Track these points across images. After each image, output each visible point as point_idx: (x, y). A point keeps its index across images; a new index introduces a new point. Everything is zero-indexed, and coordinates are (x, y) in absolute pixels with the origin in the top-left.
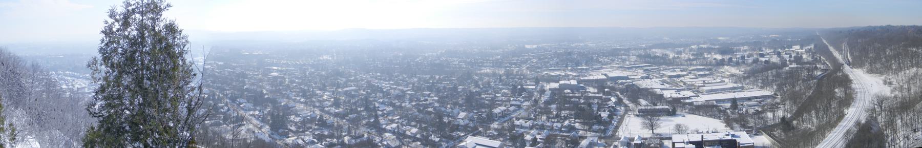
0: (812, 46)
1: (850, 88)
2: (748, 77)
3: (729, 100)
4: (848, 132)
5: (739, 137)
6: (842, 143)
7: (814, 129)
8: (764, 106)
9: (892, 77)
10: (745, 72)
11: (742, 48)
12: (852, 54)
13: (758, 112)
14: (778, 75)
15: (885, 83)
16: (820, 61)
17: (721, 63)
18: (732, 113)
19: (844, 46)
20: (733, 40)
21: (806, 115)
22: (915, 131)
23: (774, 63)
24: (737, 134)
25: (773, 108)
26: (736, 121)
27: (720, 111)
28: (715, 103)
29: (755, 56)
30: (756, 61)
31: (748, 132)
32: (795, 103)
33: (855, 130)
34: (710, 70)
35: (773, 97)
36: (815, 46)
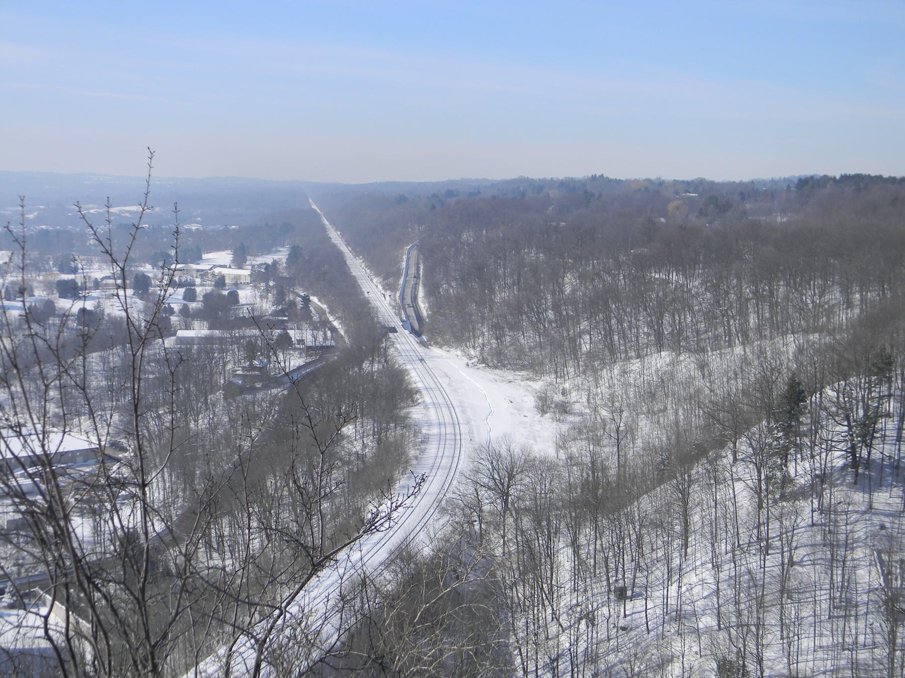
0: (281, 256)
1: (403, 422)
9: (576, 389)
12: (432, 291)
14: (133, 369)
15: (544, 405)
16: (304, 316)
19: (408, 258)
22: (622, 595)
25: (102, 492)
29: (40, 293)
36: (294, 255)
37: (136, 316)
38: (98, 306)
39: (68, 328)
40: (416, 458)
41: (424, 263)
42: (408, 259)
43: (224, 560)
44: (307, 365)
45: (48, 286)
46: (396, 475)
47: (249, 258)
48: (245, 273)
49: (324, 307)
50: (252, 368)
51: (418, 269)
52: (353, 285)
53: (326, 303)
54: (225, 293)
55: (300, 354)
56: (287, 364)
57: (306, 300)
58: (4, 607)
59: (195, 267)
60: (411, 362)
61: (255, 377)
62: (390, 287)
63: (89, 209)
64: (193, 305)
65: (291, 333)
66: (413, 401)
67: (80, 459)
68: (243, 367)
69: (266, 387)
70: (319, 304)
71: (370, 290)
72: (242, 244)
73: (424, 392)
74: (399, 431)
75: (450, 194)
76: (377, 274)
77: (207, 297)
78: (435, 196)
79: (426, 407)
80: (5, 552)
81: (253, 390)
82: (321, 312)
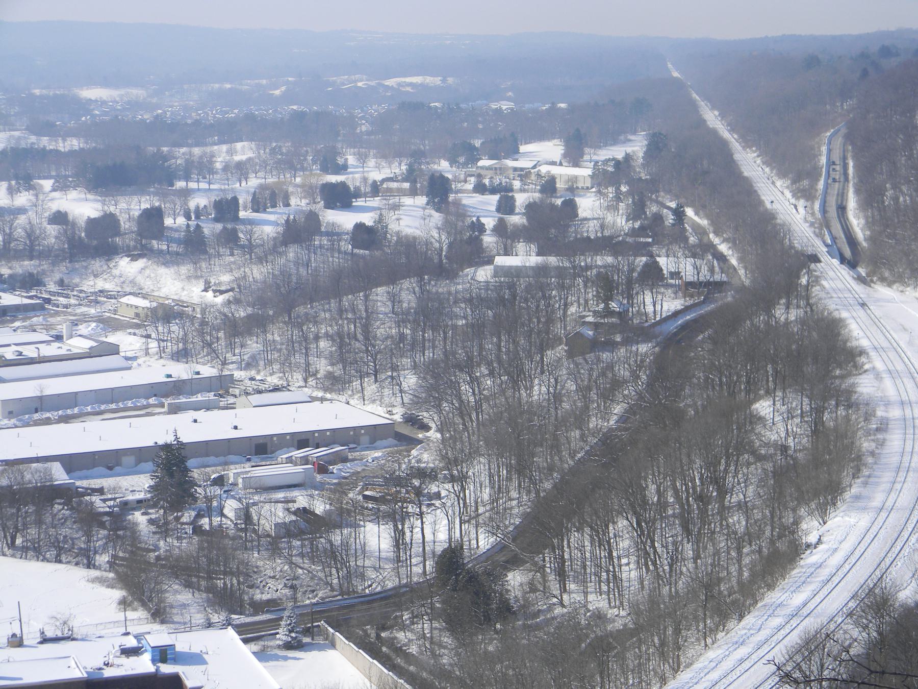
0: (636, 146)
1: (847, 399)
2: (256, 324)
3: (140, 455)
4: (813, 645)
5: (196, 659)
6: (911, 292)
7: (619, 617)
8: (341, 489)
10: (240, 291)
11: (221, 154)
12: (871, 199)
13: (308, 524)
14: (430, 314)
16: (676, 235)
17: (97, 243)
18: (163, 529)
19: (827, 147)
20: (172, 106)
21: (578, 543)
23: (409, 245)
24: (184, 643)
25: (398, 497)
26: (184, 571)
27: (90, 519)
28: (60, 475)
29: (299, 203)
30: (301, 231)
31: (249, 634)
32: (522, 469)
33: (857, 637)
34: (30, 282)
35: (400, 436)
36: (655, 147)
37: (436, 235)
38: (380, 220)
39: (339, 252)
40: (872, 454)
41: (856, 158)
42: (830, 151)
43: (586, 593)
44: (687, 309)
45: (309, 191)
46: (846, 481)
47: (587, 150)
48: (584, 172)
49: (704, 222)
50: (608, 313)
51: (845, 167)
52: (746, 193)
53: (707, 217)
54: (559, 202)
55: (675, 293)
56: (658, 307)
57: (679, 214)
58: (279, 647)
59: (510, 163)
60: (847, 307)
61: (613, 325)
62: (807, 194)
63: (356, 81)
64: (516, 219)
65: (662, 261)
66: (855, 366)
67: (365, 439)
68: (594, 312)
69: (627, 342)
70: (696, 218)
71: (773, 198)
72: (578, 130)
73: (872, 354)
74: (841, 412)
75: (886, 52)
76: (782, 175)
77: (531, 208)
78: (864, 55)
79: (878, 377)
80: (273, 569)
81: (611, 345)
82: (700, 231)
